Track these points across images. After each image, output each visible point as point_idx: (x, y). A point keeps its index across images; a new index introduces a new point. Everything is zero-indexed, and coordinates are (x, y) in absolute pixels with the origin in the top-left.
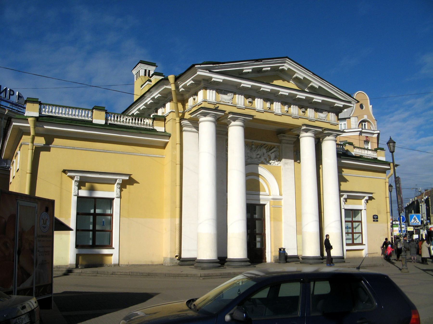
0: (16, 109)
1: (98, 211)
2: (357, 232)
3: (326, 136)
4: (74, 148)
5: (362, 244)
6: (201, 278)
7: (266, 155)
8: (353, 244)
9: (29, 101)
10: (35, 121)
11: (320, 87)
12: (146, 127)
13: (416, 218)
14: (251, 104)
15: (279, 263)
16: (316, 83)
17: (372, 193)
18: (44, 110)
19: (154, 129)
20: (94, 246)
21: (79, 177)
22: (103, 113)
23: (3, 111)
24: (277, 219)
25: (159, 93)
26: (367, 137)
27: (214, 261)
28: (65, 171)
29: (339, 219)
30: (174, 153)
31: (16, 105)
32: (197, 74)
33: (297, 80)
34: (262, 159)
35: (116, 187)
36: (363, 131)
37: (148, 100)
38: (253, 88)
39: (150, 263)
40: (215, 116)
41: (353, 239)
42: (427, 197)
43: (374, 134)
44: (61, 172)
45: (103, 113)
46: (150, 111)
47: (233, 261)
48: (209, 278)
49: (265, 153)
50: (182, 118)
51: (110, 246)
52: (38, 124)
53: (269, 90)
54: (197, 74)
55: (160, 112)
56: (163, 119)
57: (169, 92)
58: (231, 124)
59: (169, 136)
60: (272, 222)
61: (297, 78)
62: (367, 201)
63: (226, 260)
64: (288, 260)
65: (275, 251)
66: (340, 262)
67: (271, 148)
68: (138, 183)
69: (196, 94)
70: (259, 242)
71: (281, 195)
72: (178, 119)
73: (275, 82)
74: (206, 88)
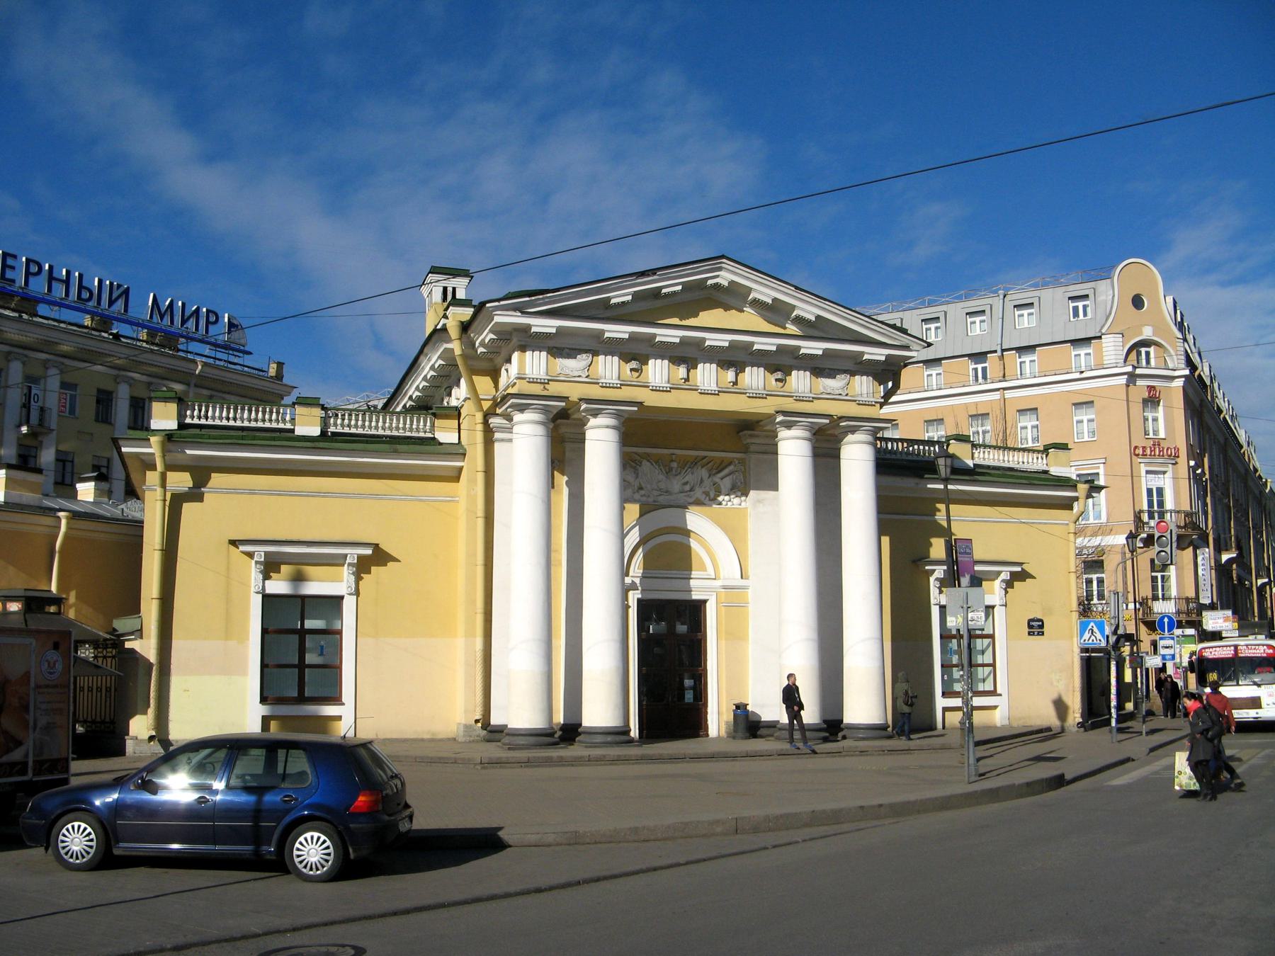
0: (225, 357)
1: (310, 624)
3: (845, 434)
4: (252, 492)
5: (993, 693)
7: (707, 482)
13: (1095, 629)
15: (734, 738)
16: (808, 309)
20: (302, 699)
23: (191, 366)
24: (736, 634)
26: (1151, 388)
28: (234, 543)
29: (877, 634)
31: (226, 347)
34: (698, 493)
35: (346, 573)
36: (1138, 371)
38: (633, 338)
39: (426, 736)
43: (1174, 378)
45: (318, 412)
47: (593, 732)
51: (336, 699)
52: (171, 446)
58: (590, 424)
60: (723, 642)
62: (1009, 584)
70: (691, 688)
72: (479, 417)
74: (523, 349)
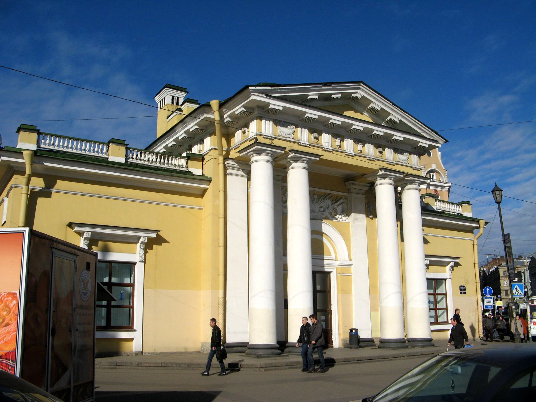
1: (114, 280)
2: (440, 307)
3: (407, 184)
4: (83, 194)
6: (263, 370)
7: (331, 207)
8: (436, 323)
9: (23, 128)
10: (32, 155)
11: (400, 121)
12: (178, 169)
13: (518, 288)
14: (317, 141)
15: (350, 348)
16: (396, 116)
17: (458, 258)
18: (43, 141)
19: (188, 171)
20: (109, 327)
21: (90, 233)
22: (123, 149)
24: (345, 291)
25: (196, 124)
26: (436, 191)
27: (271, 346)
28: (71, 225)
30: (215, 203)
32: (251, 99)
33: (373, 112)
34: (327, 213)
35: (138, 247)
36: (431, 183)
37: (181, 134)
39: (183, 351)
40: (273, 155)
41: (437, 317)
42: (496, 267)
43: (444, 187)
44: (65, 226)
46: (182, 148)
48: (272, 369)
49: (330, 205)
50: (226, 158)
51: (130, 327)
52: (36, 159)
53: (340, 123)
54: (251, 99)
55: (195, 150)
56: (200, 158)
57: (212, 122)
58: (292, 166)
59: (209, 181)
60: (340, 295)
61: (373, 109)
63: (287, 345)
64: (361, 344)
65: (344, 332)
66: (429, 346)
67: (338, 199)
68: (168, 242)
69: (247, 126)
71: (350, 259)
72: (221, 159)
73: (346, 113)
74: (260, 118)
